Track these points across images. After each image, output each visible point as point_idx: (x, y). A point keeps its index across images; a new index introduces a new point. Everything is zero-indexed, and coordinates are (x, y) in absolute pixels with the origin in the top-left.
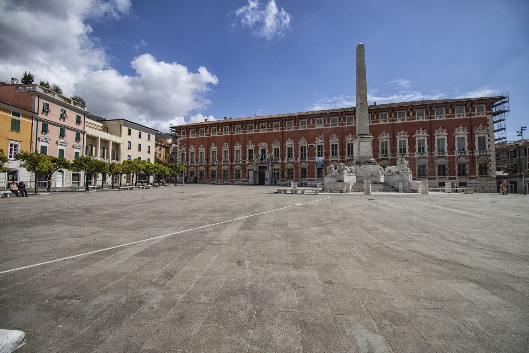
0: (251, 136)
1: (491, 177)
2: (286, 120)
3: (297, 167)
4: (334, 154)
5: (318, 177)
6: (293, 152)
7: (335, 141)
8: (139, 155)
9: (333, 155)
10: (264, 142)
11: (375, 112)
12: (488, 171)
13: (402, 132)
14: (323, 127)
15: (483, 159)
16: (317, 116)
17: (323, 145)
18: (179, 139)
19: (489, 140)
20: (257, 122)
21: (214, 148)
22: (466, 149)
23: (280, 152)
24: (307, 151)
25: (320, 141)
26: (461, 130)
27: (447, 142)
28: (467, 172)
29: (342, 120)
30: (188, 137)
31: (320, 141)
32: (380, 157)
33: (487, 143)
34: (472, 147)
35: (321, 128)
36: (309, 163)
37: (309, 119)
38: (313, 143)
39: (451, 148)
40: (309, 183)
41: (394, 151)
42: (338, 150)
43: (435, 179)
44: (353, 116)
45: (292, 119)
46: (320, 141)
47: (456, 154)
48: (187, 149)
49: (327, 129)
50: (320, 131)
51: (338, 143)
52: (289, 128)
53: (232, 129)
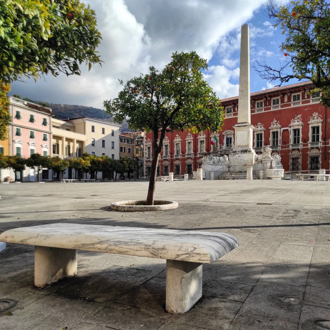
6: (263, 140)
8: (103, 150)
14: (301, 105)
17: (301, 128)
24: (280, 138)
25: (296, 123)
31: (296, 123)
35: (262, 112)
37: (284, 96)
42: (263, 140)
45: (262, 99)
46: (296, 123)
49: (306, 107)
50: (296, 111)
51: (320, 125)
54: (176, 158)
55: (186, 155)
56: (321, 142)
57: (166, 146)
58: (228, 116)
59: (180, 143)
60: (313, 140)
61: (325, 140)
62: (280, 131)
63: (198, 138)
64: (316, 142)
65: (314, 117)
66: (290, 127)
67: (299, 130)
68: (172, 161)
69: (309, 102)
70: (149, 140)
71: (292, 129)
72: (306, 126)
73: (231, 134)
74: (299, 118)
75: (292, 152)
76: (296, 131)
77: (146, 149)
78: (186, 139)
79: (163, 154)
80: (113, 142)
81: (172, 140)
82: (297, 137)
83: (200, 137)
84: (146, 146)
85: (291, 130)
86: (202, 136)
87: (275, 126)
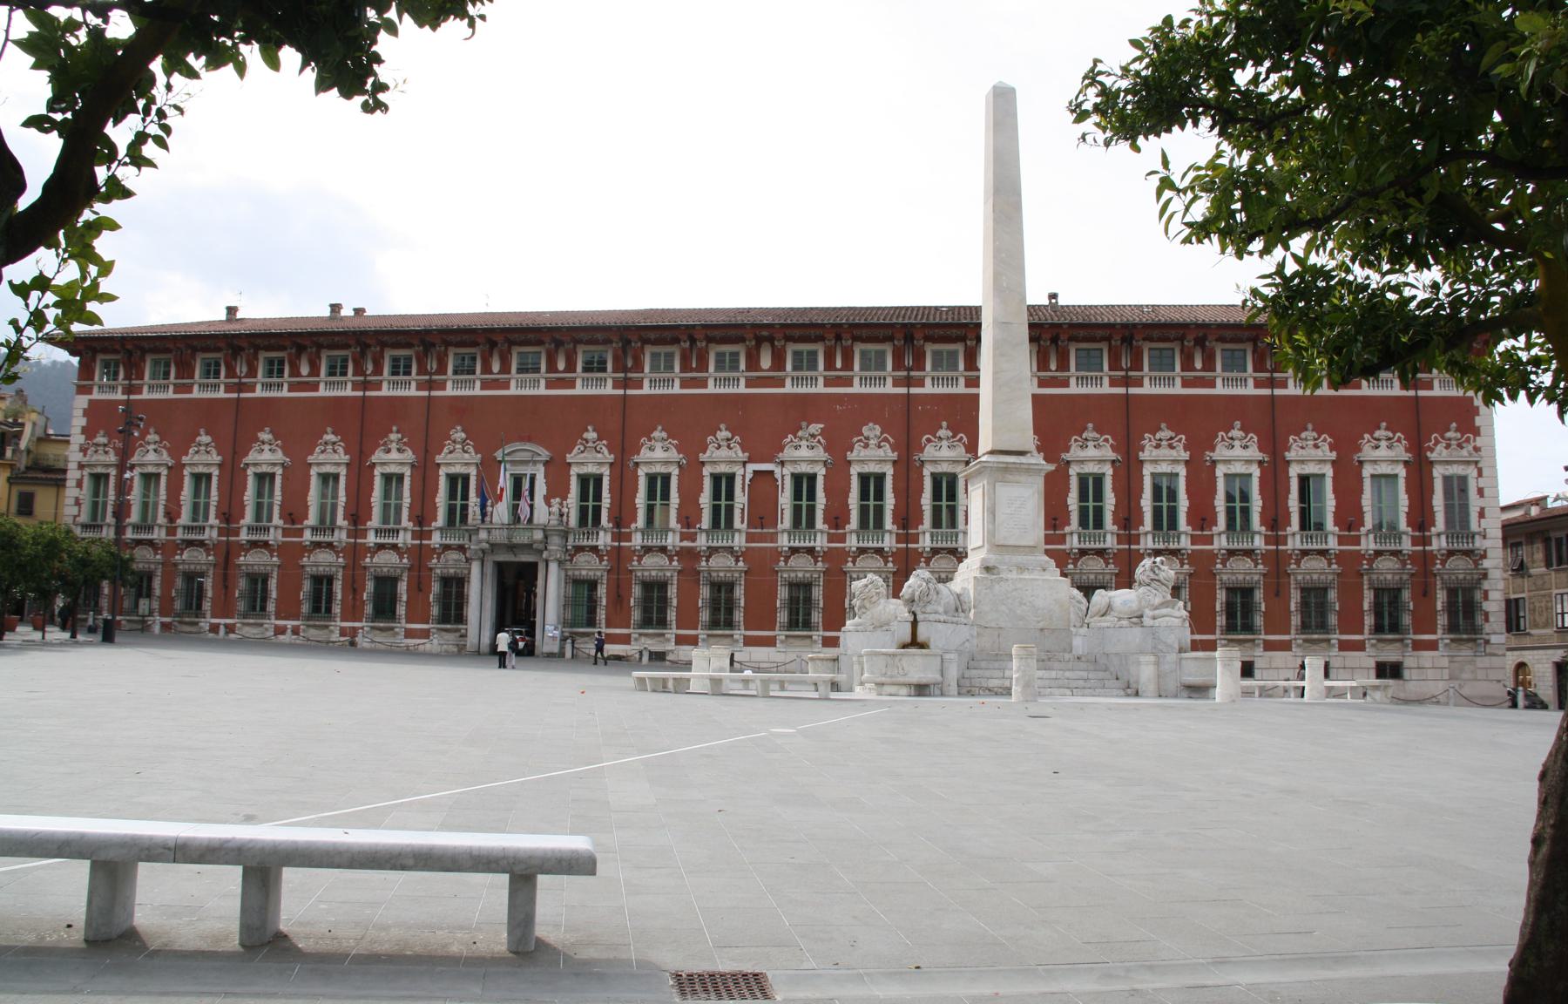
0: (462, 409)
1: (1487, 642)
2: (646, 341)
4: (871, 520)
5: (714, 624)
6: (1183, 503)
7: (873, 454)
9: (864, 523)
10: (529, 439)
11: (1055, 340)
12: (1479, 619)
13: (1165, 434)
14: (820, 388)
15: (1459, 566)
16: (652, 336)
19: (1481, 492)
20: (499, 338)
21: (151, 457)
22: (1403, 525)
23: (606, 494)
24: (741, 499)
25: (804, 453)
26: (1383, 444)
27: (1335, 491)
28: (1407, 620)
29: (909, 361)
30: (129, 390)
31: (804, 452)
32: (1074, 543)
33: (1475, 503)
34: (1421, 518)
35: (670, 391)
36: (746, 554)
38: (770, 461)
39: (1349, 518)
41: (1128, 519)
42: (1183, 503)
43: (1360, 646)
44: (959, 348)
46: (804, 452)
47: (1368, 544)
50: (804, 408)
53: (370, 368)
54: (251, 537)
55: (180, 531)
57: (328, 479)
58: (521, 384)
59: (279, 471)
61: (228, 521)
62: (744, 475)
63: (374, 459)
65: (867, 438)
66: (782, 463)
68: (228, 553)
69: (571, 384)
70: (101, 439)
71: (788, 470)
72: (838, 468)
74: (813, 436)
75: (787, 559)
76: (805, 484)
77: (1482, 514)
78: (310, 459)
79: (179, 516)
81: (361, 452)
82: (459, 502)
83: (1228, 454)
84: (81, 466)
85: (784, 475)
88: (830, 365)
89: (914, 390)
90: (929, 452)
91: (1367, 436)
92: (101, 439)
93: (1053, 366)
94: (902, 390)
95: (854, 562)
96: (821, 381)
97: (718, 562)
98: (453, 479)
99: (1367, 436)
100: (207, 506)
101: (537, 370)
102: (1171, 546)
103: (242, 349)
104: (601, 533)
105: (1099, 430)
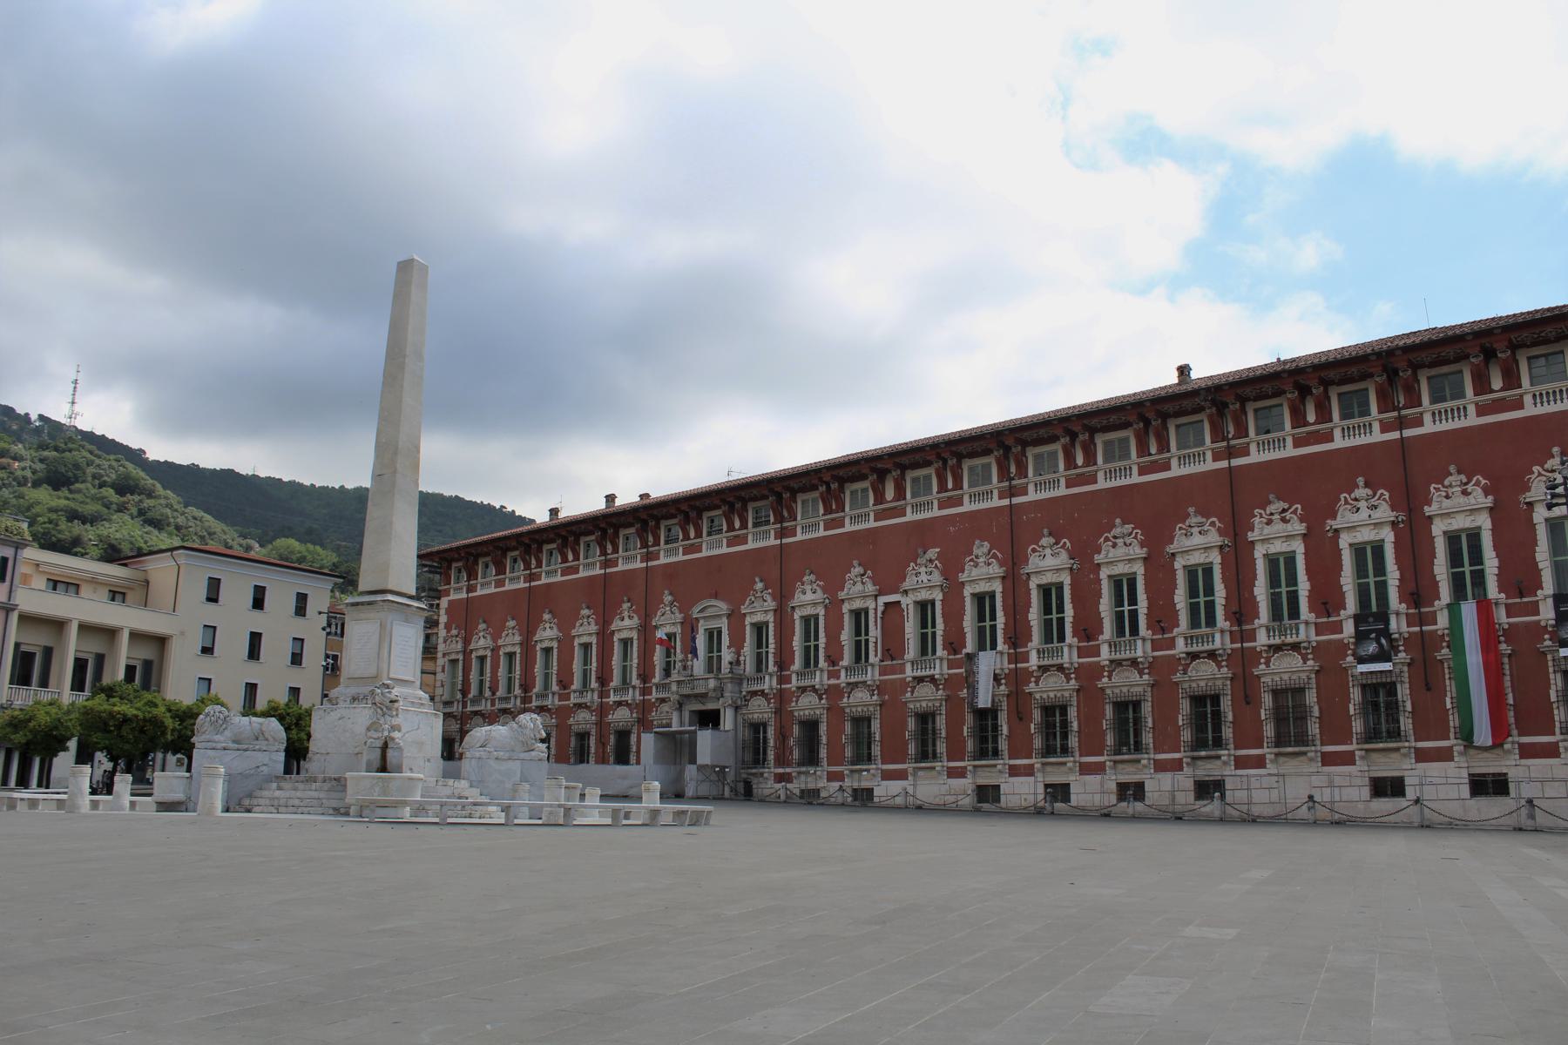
0: (671, 571)
3: (1163, 687)
6: (1304, 586)
18: (444, 602)
23: (822, 634)
24: (875, 632)
25: (924, 581)
36: (880, 688)
38: (895, 592)
40: (885, 790)
42: (1304, 586)
43: (1348, 759)
48: (467, 642)
50: (923, 534)
52: (629, 561)
56: (1144, 640)
60: (1276, 615)
62: (876, 607)
64: (1286, 621)
66: (906, 592)
67: (1060, 587)
70: (454, 632)
73: (719, 616)
74: (931, 561)
76: (924, 607)
78: (574, 632)
80: (300, 641)
82: (1284, 589)
86: (627, 622)
87: (859, 587)
88: (943, 488)
89: (1236, 462)
90: (1034, 562)
91: (1536, 469)
92: (454, 632)
93: (1153, 450)
94: (1224, 464)
95: (1037, 683)
96: (1376, 426)
97: (861, 696)
98: (1117, 582)
99: (1536, 469)
100: (1061, 622)
101: (767, 523)
102: (1289, 640)
103: (888, 471)
104: (1139, 643)
105: (1057, 535)
